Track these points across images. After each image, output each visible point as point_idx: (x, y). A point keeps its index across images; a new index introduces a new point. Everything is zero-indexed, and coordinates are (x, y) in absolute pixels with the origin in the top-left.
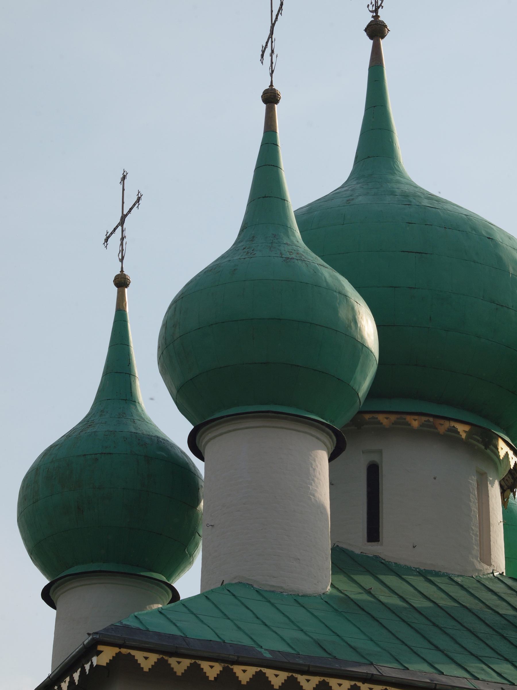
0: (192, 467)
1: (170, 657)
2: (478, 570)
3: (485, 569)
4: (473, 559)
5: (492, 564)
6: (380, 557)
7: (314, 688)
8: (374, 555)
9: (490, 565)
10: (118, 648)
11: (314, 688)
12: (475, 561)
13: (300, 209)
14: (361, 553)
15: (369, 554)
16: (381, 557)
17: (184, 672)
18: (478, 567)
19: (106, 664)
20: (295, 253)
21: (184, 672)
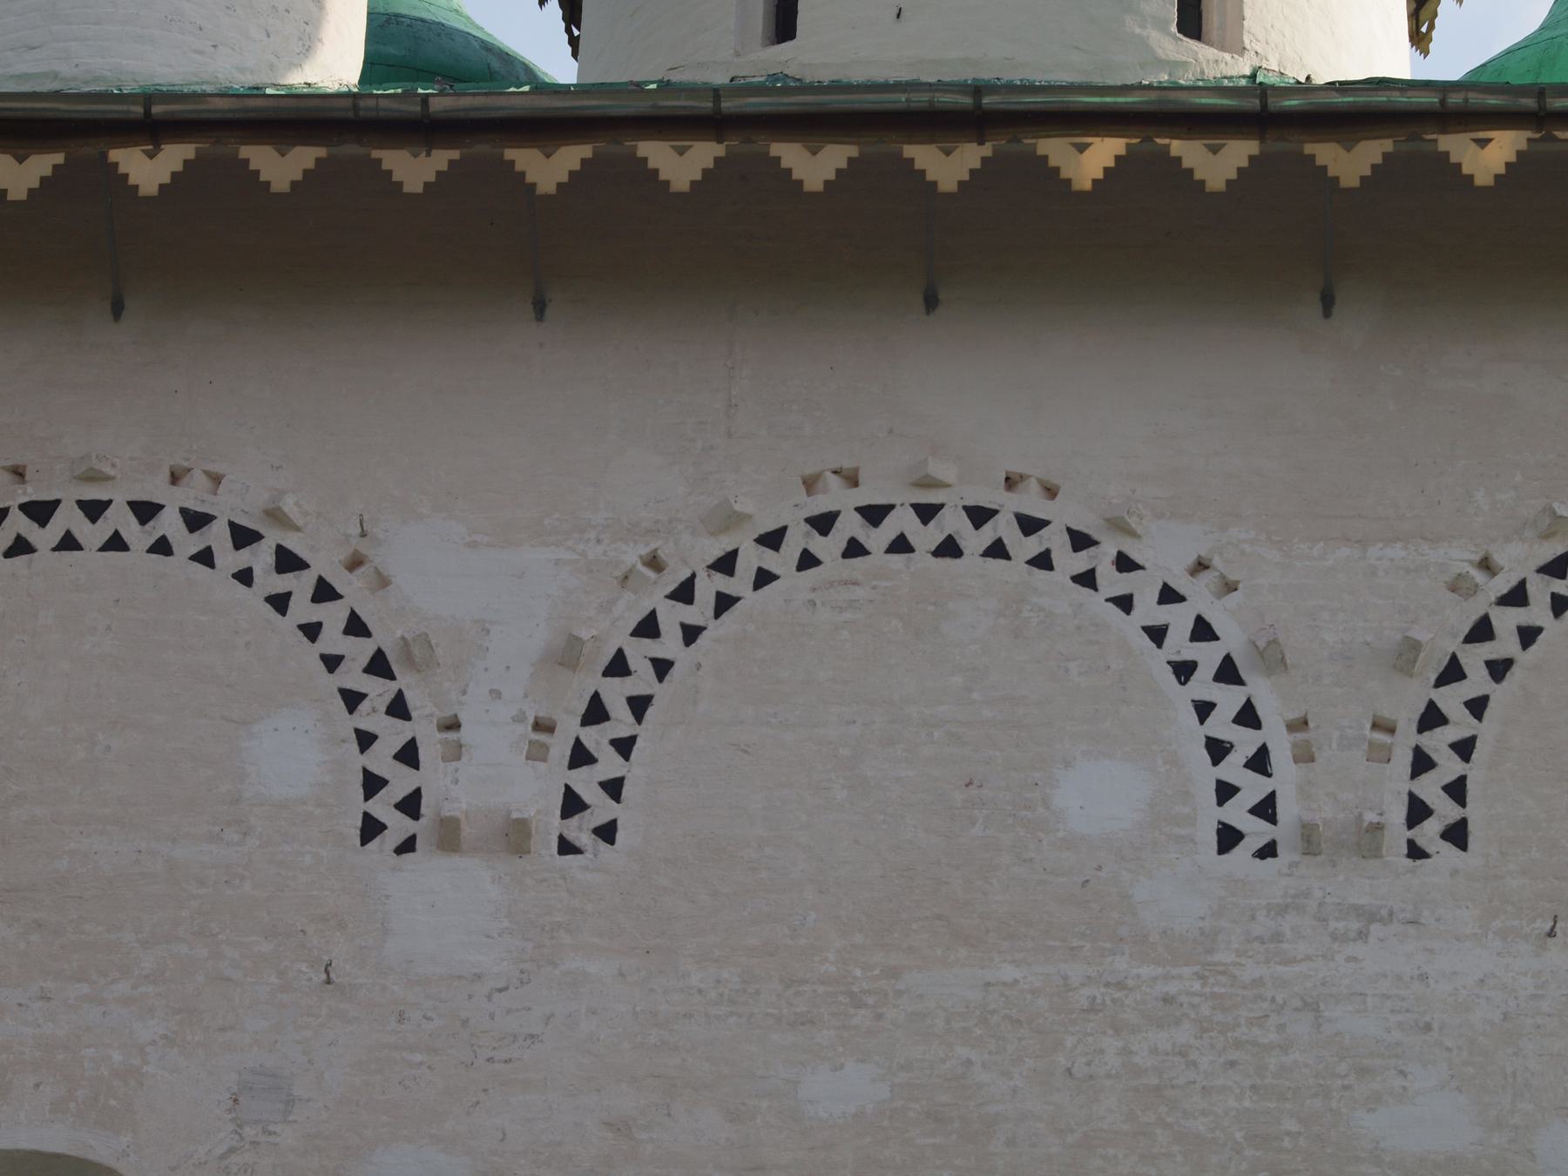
0: (931, 102)
1: (1444, 132)
2: (1168, 62)
3: (1208, 61)
4: (1143, 27)
5: (1248, 47)
6: (786, 75)
7: (5, 192)
8: (769, 75)
9: (1242, 50)
10: (974, 145)
11: (5, 192)
12: (1154, 36)
13: (1366, 83)
14: (731, 81)
15: (753, 77)
16: (790, 75)
17: (445, 169)
18: (1167, 55)
19: (41, 182)
20: (976, 1025)
21: (445, 169)
